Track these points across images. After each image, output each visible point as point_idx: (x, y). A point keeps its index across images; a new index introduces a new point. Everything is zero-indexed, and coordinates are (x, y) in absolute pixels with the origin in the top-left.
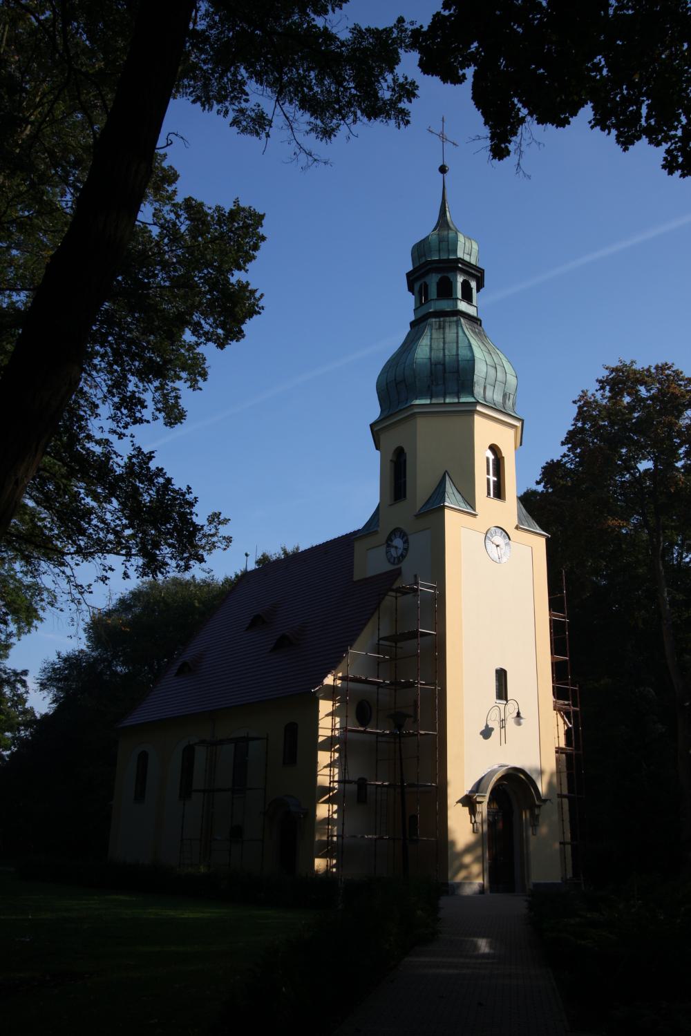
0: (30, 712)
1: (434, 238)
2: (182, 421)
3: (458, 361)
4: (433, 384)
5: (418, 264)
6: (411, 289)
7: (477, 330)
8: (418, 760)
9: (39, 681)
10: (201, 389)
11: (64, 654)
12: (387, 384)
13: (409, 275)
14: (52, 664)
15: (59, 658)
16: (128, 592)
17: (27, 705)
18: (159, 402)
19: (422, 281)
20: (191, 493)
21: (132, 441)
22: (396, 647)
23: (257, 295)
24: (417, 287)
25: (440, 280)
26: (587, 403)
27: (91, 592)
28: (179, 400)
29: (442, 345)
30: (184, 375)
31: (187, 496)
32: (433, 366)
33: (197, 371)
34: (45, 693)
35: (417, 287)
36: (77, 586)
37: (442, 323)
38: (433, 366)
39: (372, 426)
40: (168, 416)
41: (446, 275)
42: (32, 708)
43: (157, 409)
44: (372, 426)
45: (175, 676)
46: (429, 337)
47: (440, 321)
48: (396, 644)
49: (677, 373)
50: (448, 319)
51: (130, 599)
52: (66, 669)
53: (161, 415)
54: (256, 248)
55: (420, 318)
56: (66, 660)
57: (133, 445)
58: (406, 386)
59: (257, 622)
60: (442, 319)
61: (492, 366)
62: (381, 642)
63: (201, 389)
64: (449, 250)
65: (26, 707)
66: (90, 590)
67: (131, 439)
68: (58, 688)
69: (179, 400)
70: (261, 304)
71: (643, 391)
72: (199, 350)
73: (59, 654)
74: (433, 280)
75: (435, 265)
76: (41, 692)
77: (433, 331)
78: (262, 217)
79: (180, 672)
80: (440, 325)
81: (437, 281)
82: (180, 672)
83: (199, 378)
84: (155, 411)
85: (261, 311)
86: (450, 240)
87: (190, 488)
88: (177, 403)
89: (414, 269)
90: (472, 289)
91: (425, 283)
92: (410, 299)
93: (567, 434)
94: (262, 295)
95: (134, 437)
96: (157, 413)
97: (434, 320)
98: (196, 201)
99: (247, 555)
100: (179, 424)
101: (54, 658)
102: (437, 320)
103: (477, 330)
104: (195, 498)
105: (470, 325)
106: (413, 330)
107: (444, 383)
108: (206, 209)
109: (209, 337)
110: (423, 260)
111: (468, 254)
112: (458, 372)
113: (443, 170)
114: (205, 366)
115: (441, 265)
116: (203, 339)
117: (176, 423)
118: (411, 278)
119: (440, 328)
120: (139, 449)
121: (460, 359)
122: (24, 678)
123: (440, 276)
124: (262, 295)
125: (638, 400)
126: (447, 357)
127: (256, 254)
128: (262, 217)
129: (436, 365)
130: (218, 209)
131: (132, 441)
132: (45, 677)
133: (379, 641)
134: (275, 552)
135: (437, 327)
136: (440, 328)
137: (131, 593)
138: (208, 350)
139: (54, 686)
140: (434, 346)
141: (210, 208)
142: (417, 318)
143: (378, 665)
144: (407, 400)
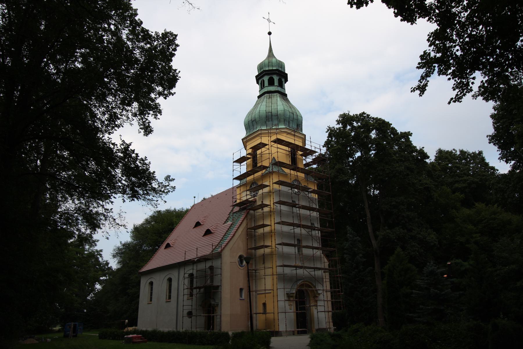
0: (110, 268)
1: (267, 61)
2: (152, 133)
3: (277, 111)
4: (267, 121)
5: (260, 72)
6: (258, 83)
7: (285, 99)
8: (265, 279)
9: (112, 254)
10: (159, 119)
11: (123, 242)
12: (248, 122)
13: (256, 77)
14: (118, 247)
15: (121, 244)
16: (149, 216)
17: (109, 266)
18: (141, 125)
19: (262, 79)
20: (147, 160)
21: (121, 138)
22: (255, 232)
23: (177, 72)
24: (260, 82)
25: (269, 78)
26: (331, 130)
27: (112, 212)
28: (150, 124)
29: (270, 104)
30: (151, 112)
31: (146, 161)
32: (267, 113)
33: (157, 110)
34: (115, 259)
35: (260, 82)
36: (105, 209)
37: (271, 96)
38: (267, 113)
39: (242, 140)
40: (145, 131)
41: (272, 76)
42: (111, 267)
43: (141, 128)
44: (242, 140)
45: (164, 249)
46: (266, 101)
47: (269, 95)
48: (255, 231)
49: (368, 115)
50: (273, 94)
51: (150, 219)
52: (124, 249)
53: (142, 131)
54: (175, 50)
55: (261, 95)
56: (124, 245)
57: (121, 140)
58: (256, 122)
59: (198, 224)
60: (270, 94)
61: (292, 113)
62: (248, 230)
63: (159, 119)
64: (272, 66)
65: (109, 266)
66: (112, 211)
67: (120, 137)
68: (120, 256)
69: (150, 124)
70: (179, 75)
71: (355, 124)
72: (157, 101)
73: (121, 242)
74: (266, 79)
75: (267, 72)
76: (114, 259)
77: (267, 99)
78: (176, 36)
79: (166, 247)
80: (270, 97)
81: (268, 78)
82: (166, 247)
83: (158, 114)
84: (139, 129)
85: (179, 78)
86: (273, 62)
87: (146, 158)
88: (149, 125)
89: (259, 74)
90: (283, 82)
91: (263, 80)
92: (258, 87)
93: (325, 143)
94: (179, 72)
95: (121, 136)
96: (141, 130)
97: (267, 95)
98: (145, 29)
99: (195, 197)
100: (150, 134)
101: (119, 245)
102: (269, 94)
103: (285, 99)
104: (150, 162)
105: (282, 96)
106: (259, 99)
107: (272, 121)
108: (150, 33)
109: (160, 94)
110: (262, 70)
111: (280, 67)
112: (277, 115)
113: (270, 33)
114: (160, 108)
115: (269, 72)
116: (158, 96)
117: (149, 134)
118: (257, 78)
119: (270, 98)
120: (123, 141)
121: (278, 110)
122: (101, 253)
123: (269, 77)
124: (179, 72)
125: (353, 128)
126: (273, 110)
127: (175, 53)
128: (176, 36)
129: (268, 113)
130: (156, 33)
131: (121, 138)
132: (115, 253)
133: (247, 230)
134: (208, 196)
135: (269, 98)
136: (270, 98)
137: (150, 216)
138: (160, 100)
139: (118, 256)
140: (267, 105)
141: (152, 32)
142: (261, 94)
143: (247, 240)
144: (257, 128)
